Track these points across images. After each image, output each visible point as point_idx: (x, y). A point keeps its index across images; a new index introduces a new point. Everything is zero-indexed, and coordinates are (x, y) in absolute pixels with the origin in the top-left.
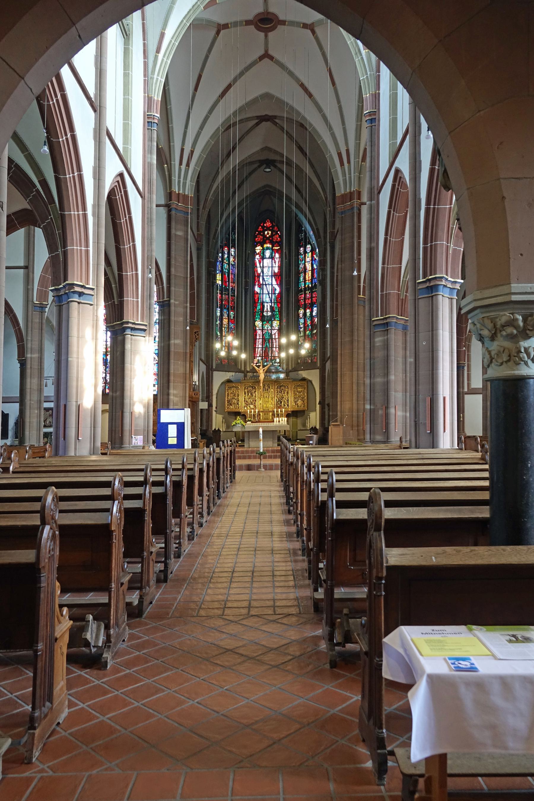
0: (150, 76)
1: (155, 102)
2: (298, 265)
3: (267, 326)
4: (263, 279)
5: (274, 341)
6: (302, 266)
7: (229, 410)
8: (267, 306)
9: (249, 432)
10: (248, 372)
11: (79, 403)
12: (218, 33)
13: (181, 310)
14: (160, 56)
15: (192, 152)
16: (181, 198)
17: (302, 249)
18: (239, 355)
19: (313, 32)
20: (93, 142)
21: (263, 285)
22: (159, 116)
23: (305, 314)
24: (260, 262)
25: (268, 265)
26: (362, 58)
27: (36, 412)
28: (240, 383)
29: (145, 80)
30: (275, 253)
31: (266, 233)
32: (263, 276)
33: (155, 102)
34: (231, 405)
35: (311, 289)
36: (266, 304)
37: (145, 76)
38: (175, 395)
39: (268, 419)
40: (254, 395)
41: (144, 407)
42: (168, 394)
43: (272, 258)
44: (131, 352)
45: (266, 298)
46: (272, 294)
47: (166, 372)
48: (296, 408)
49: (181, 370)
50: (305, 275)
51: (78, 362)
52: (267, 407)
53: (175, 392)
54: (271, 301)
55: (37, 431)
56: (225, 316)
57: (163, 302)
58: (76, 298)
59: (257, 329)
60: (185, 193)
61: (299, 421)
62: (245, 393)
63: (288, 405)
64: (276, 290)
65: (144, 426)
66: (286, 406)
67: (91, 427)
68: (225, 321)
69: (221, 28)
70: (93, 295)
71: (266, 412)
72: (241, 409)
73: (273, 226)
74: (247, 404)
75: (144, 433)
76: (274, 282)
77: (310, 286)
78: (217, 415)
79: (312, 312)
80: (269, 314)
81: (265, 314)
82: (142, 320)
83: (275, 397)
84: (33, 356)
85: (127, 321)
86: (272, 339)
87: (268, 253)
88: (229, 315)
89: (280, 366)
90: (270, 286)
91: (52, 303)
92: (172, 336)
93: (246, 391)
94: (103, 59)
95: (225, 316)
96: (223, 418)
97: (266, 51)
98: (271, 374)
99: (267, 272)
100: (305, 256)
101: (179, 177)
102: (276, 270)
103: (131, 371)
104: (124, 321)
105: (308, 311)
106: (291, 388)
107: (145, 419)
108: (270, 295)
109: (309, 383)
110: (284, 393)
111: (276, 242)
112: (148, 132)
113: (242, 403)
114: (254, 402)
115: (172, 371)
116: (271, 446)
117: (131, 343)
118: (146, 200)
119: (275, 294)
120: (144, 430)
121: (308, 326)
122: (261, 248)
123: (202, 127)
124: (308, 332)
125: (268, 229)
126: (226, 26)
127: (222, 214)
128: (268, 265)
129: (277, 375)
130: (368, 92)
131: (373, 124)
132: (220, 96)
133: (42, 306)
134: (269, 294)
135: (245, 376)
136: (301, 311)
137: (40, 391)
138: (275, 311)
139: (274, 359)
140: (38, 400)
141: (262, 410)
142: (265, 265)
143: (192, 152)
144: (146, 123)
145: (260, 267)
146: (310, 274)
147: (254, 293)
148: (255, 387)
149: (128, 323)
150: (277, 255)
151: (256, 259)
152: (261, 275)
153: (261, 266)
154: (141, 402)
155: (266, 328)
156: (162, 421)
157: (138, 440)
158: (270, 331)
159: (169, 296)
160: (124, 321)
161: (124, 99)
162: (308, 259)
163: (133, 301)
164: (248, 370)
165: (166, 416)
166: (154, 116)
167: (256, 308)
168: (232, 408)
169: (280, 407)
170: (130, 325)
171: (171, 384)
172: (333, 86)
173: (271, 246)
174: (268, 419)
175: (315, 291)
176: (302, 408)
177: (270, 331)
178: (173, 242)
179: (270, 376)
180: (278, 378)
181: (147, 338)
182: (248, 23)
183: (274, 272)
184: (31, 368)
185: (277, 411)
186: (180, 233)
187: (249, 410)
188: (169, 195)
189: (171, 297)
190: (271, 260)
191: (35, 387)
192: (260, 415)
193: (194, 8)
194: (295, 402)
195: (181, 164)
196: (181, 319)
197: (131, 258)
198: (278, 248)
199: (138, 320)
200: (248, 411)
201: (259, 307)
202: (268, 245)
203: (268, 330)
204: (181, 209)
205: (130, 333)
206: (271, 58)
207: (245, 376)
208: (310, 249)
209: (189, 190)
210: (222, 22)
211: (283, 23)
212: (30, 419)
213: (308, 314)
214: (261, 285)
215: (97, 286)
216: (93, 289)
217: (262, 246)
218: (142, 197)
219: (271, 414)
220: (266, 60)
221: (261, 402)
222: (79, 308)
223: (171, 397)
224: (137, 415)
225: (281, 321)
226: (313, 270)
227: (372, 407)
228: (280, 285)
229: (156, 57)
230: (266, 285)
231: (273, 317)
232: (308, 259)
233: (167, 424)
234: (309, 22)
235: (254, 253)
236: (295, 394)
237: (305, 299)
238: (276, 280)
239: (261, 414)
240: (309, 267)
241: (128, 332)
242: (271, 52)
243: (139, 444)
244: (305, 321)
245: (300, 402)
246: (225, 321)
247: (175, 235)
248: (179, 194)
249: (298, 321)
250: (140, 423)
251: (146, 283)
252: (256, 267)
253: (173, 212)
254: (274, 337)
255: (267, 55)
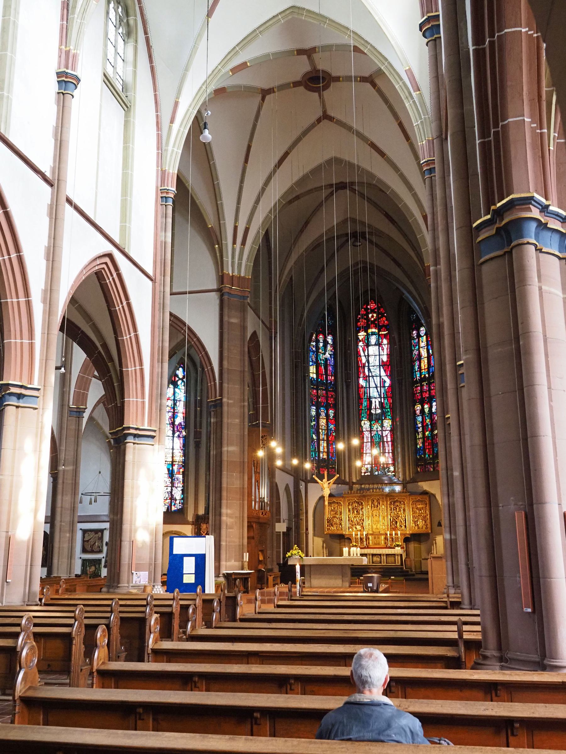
0: (164, 148)
1: (171, 175)
2: (412, 351)
3: (376, 426)
4: (369, 370)
5: (386, 444)
6: (415, 352)
7: (330, 532)
8: (376, 403)
9: (310, 565)
10: (354, 483)
11: (10, 533)
12: (263, 99)
13: (236, 410)
14: (176, 126)
15: (247, 230)
16: (235, 282)
17: (414, 332)
18: (302, 463)
19: (374, 85)
20: (47, 219)
21: (369, 376)
22: (174, 189)
23: (422, 411)
24: (364, 351)
25: (374, 354)
26: (414, 102)
27: (68, 535)
28: (343, 497)
29: (158, 153)
30: (382, 339)
31: (370, 315)
32: (369, 366)
33: (171, 175)
34: (332, 525)
35: (430, 379)
36: (373, 400)
37: (158, 149)
38: (227, 515)
39: (379, 544)
40: (361, 513)
41: (151, 534)
42: (220, 515)
43: (379, 344)
44: (134, 464)
45: (374, 393)
46: (381, 387)
47: (218, 486)
48: (416, 530)
49: (237, 484)
50: (420, 363)
51: (12, 482)
52: (377, 529)
53: (229, 511)
54: (380, 395)
55: (68, 559)
56: (323, 414)
57: (215, 401)
58: (13, 401)
59: (364, 430)
60: (240, 275)
61: (423, 547)
62: (349, 511)
63: (405, 526)
64: (385, 382)
65: (150, 559)
66: (403, 527)
67: (27, 566)
68: (323, 422)
69: (265, 93)
70: (38, 397)
71: (376, 535)
72: (345, 531)
73: (379, 308)
74: (352, 524)
75: (149, 568)
76: (383, 373)
77: (427, 375)
78: (316, 538)
79: (431, 408)
80: (379, 411)
81: (373, 411)
82: (150, 423)
83: (387, 516)
84: (67, 468)
85: (128, 426)
86: (383, 442)
87: (373, 340)
88: (327, 415)
89: (394, 475)
90: (379, 378)
91: (96, 406)
92: (225, 442)
93: (350, 507)
94: (65, 129)
95: (323, 414)
96: (324, 542)
97: (325, 112)
98: (384, 486)
99: (375, 361)
100: (419, 340)
101: (233, 257)
102: (385, 359)
103: (133, 488)
104: (124, 426)
105: (426, 406)
106: (408, 504)
107: (151, 549)
108: (379, 389)
109: (432, 498)
110: (400, 511)
111: (383, 326)
112: (162, 208)
113: (346, 524)
114: (361, 522)
115: (224, 485)
116: (340, 585)
117: (134, 453)
118: (156, 284)
119: (384, 387)
120: (150, 564)
121: (427, 425)
122: (365, 334)
123: (257, 201)
124: (427, 433)
125: (373, 311)
126: (270, 91)
127: (308, 298)
128: (374, 354)
129: (392, 487)
130: (424, 139)
131: (432, 175)
132: (276, 166)
133: (79, 410)
134: (376, 387)
135: (351, 489)
136: (418, 407)
137: (74, 509)
138: (385, 408)
139: (387, 467)
140: (70, 521)
141: (371, 532)
142: (371, 353)
143: (247, 230)
144: (160, 199)
145: (365, 356)
146: (426, 361)
147: (359, 387)
148: (362, 503)
149: (129, 428)
150: (385, 341)
151: (360, 347)
152: (367, 365)
153: (366, 354)
154: (146, 527)
155: (375, 428)
156: (174, 553)
157: (141, 578)
158: (380, 433)
159: (221, 395)
160: (124, 426)
161: (123, 173)
162: (423, 344)
163: (137, 401)
164: (354, 481)
165: (182, 546)
166: (168, 190)
167: (362, 404)
168: (334, 529)
169: (395, 529)
170: (132, 431)
171: (224, 502)
172: (407, 141)
173: (377, 331)
174: (379, 544)
175: (433, 382)
176: (423, 530)
177: (380, 433)
178: (225, 330)
179: (383, 489)
180: (393, 491)
181: (156, 446)
182: (296, 84)
183: (382, 361)
184: (63, 482)
185: (391, 535)
186: (234, 320)
187: (354, 533)
188: (221, 278)
189: (223, 395)
190: (377, 347)
191: (67, 505)
192: (369, 538)
193: (215, 73)
194: (415, 522)
195: (234, 242)
196: (237, 421)
197: (133, 351)
198: (385, 333)
199: (143, 425)
200: (354, 533)
201: (365, 404)
202: (374, 330)
203: (377, 431)
204: (236, 293)
205: (133, 441)
206: (331, 119)
207: (351, 489)
208: (425, 331)
209: (245, 271)
210: (266, 86)
211: (337, 79)
212: (60, 545)
213: (427, 410)
214: (367, 377)
215: (44, 386)
216: (38, 390)
217: (366, 331)
218: (152, 280)
219: (383, 537)
220: (325, 122)
221: (370, 522)
222: (17, 413)
223: (224, 518)
224: (140, 545)
225: (393, 419)
226: (429, 357)
227: (453, 537)
228: (390, 377)
229: (170, 128)
230: (373, 376)
231: (383, 414)
232: (423, 344)
233: (181, 557)
234: (367, 74)
235: (357, 340)
236: (414, 512)
237: (422, 391)
238: (385, 371)
239: (370, 537)
240: (424, 353)
241: (130, 439)
242: (331, 113)
243: (142, 583)
244: (423, 418)
245: (421, 523)
246: (323, 422)
247: (229, 323)
248: (233, 276)
249: (415, 420)
250: (145, 556)
251: (155, 379)
252: (361, 356)
253: (226, 297)
254: (385, 440)
255: (326, 117)
